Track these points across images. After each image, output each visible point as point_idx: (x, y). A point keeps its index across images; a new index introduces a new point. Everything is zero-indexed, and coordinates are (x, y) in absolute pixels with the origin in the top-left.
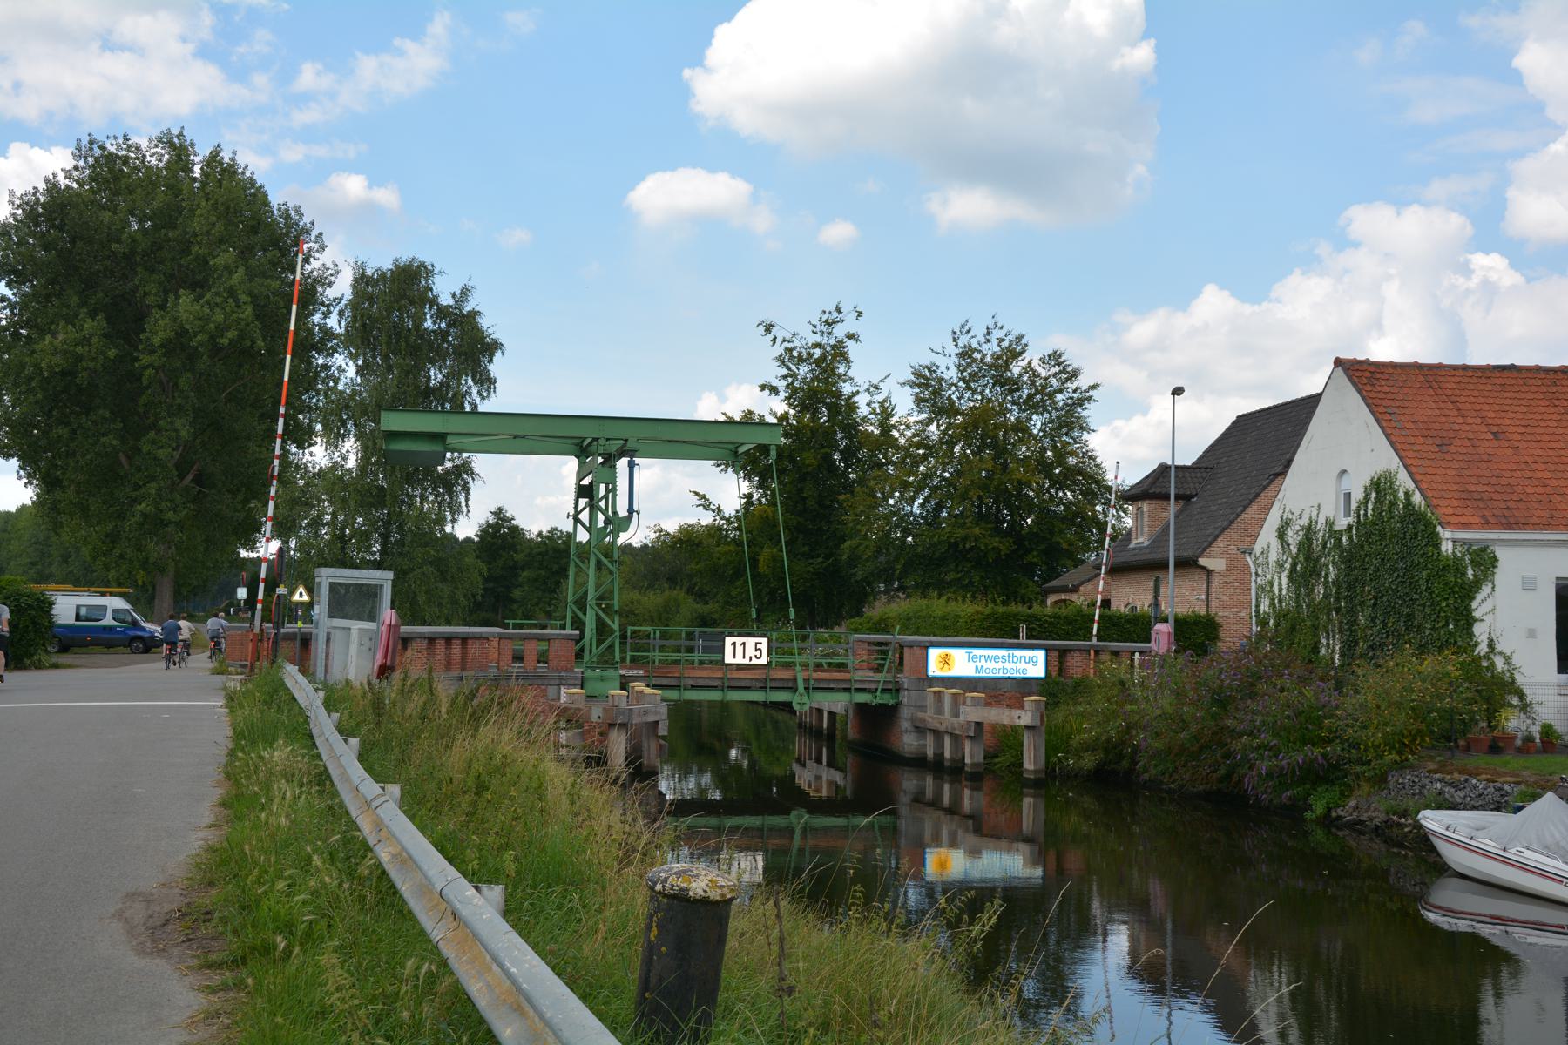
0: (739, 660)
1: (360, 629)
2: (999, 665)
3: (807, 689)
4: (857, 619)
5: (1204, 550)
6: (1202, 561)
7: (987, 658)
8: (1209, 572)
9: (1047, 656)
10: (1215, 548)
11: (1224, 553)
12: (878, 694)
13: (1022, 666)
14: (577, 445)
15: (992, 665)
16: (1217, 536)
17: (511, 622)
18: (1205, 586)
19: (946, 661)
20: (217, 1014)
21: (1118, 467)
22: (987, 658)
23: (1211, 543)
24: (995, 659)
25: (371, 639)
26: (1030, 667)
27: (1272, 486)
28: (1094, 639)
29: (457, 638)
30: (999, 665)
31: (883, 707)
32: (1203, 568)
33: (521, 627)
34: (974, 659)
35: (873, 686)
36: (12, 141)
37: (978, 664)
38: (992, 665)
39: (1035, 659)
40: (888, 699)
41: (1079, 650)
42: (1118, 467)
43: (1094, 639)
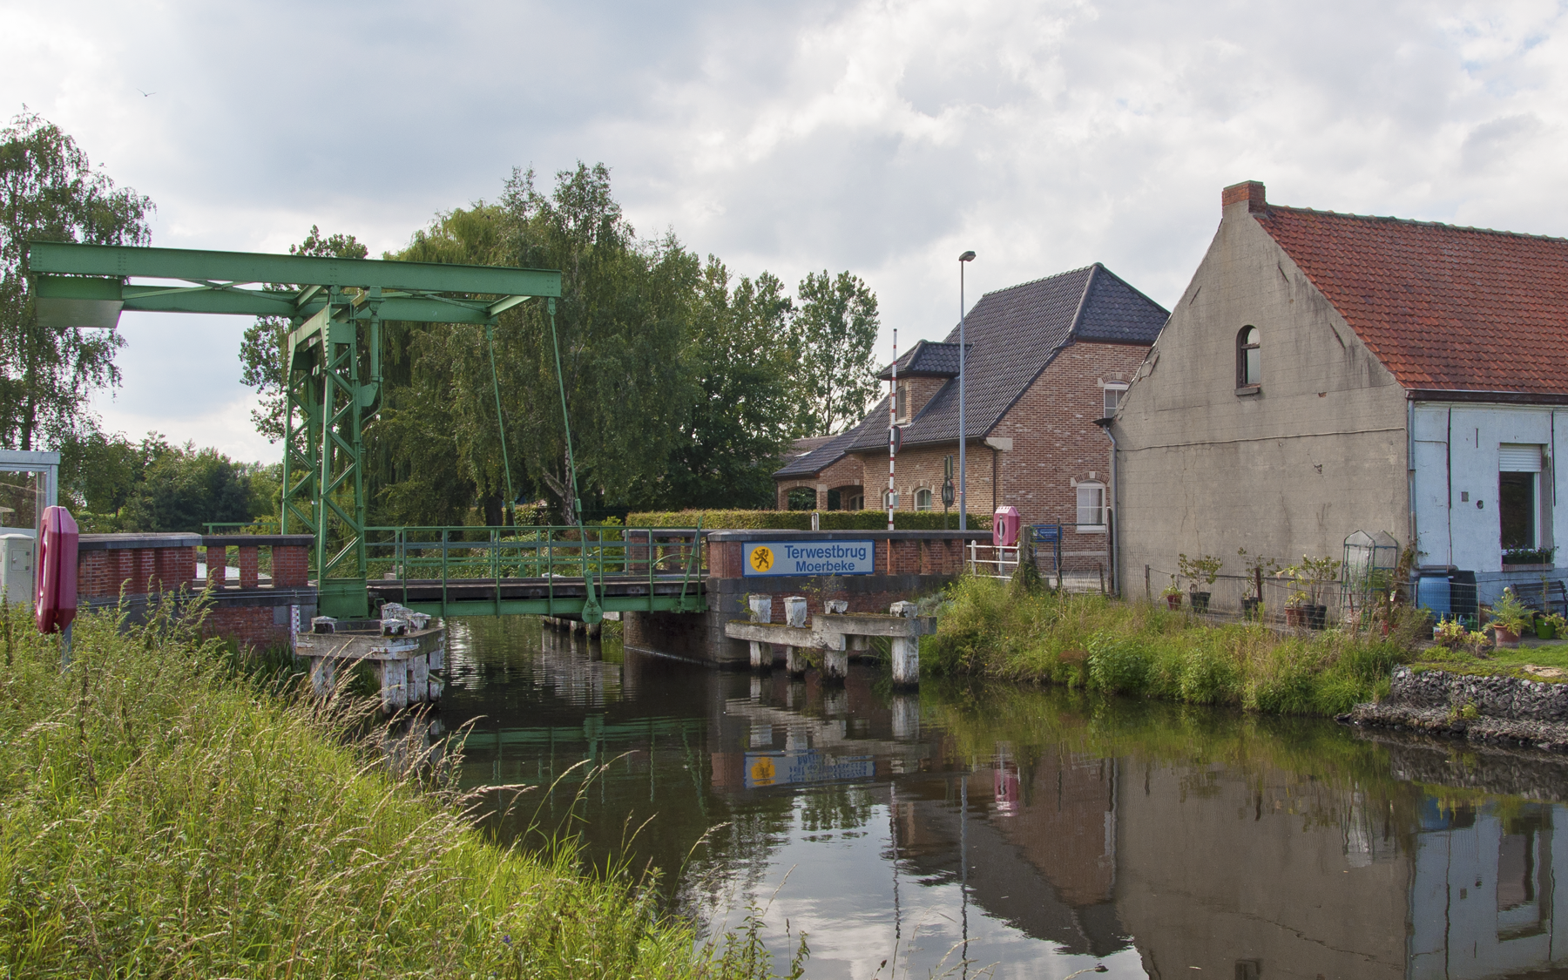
0: (763, 570)
1: (9, 539)
2: (823, 560)
3: (598, 596)
4: (1518, 583)
5: (992, 427)
6: (990, 441)
7: (811, 554)
8: (995, 452)
9: (875, 548)
10: (1002, 428)
11: (1012, 432)
12: (682, 599)
13: (848, 560)
14: (291, 302)
15: (815, 561)
16: (1004, 413)
17: (210, 525)
18: (990, 465)
19: (762, 557)
20: (787, 818)
21: (895, 336)
22: (811, 554)
23: (999, 420)
24: (818, 553)
25: (28, 554)
26: (856, 561)
27: (1056, 361)
28: (891, 527)
29: (149, 549)
30: (823, 560)
31: (689, 615)
32: (990, 448)
33: (224, 530)
34: (795, 554)
35: (676, 590)
36: (639, 263)
37: (799, 559)
38: (815, 561)
39: (862, 552)
40: (686, 605)
41: (910, 540)
42: (895, 336)
43: (891, 527)
